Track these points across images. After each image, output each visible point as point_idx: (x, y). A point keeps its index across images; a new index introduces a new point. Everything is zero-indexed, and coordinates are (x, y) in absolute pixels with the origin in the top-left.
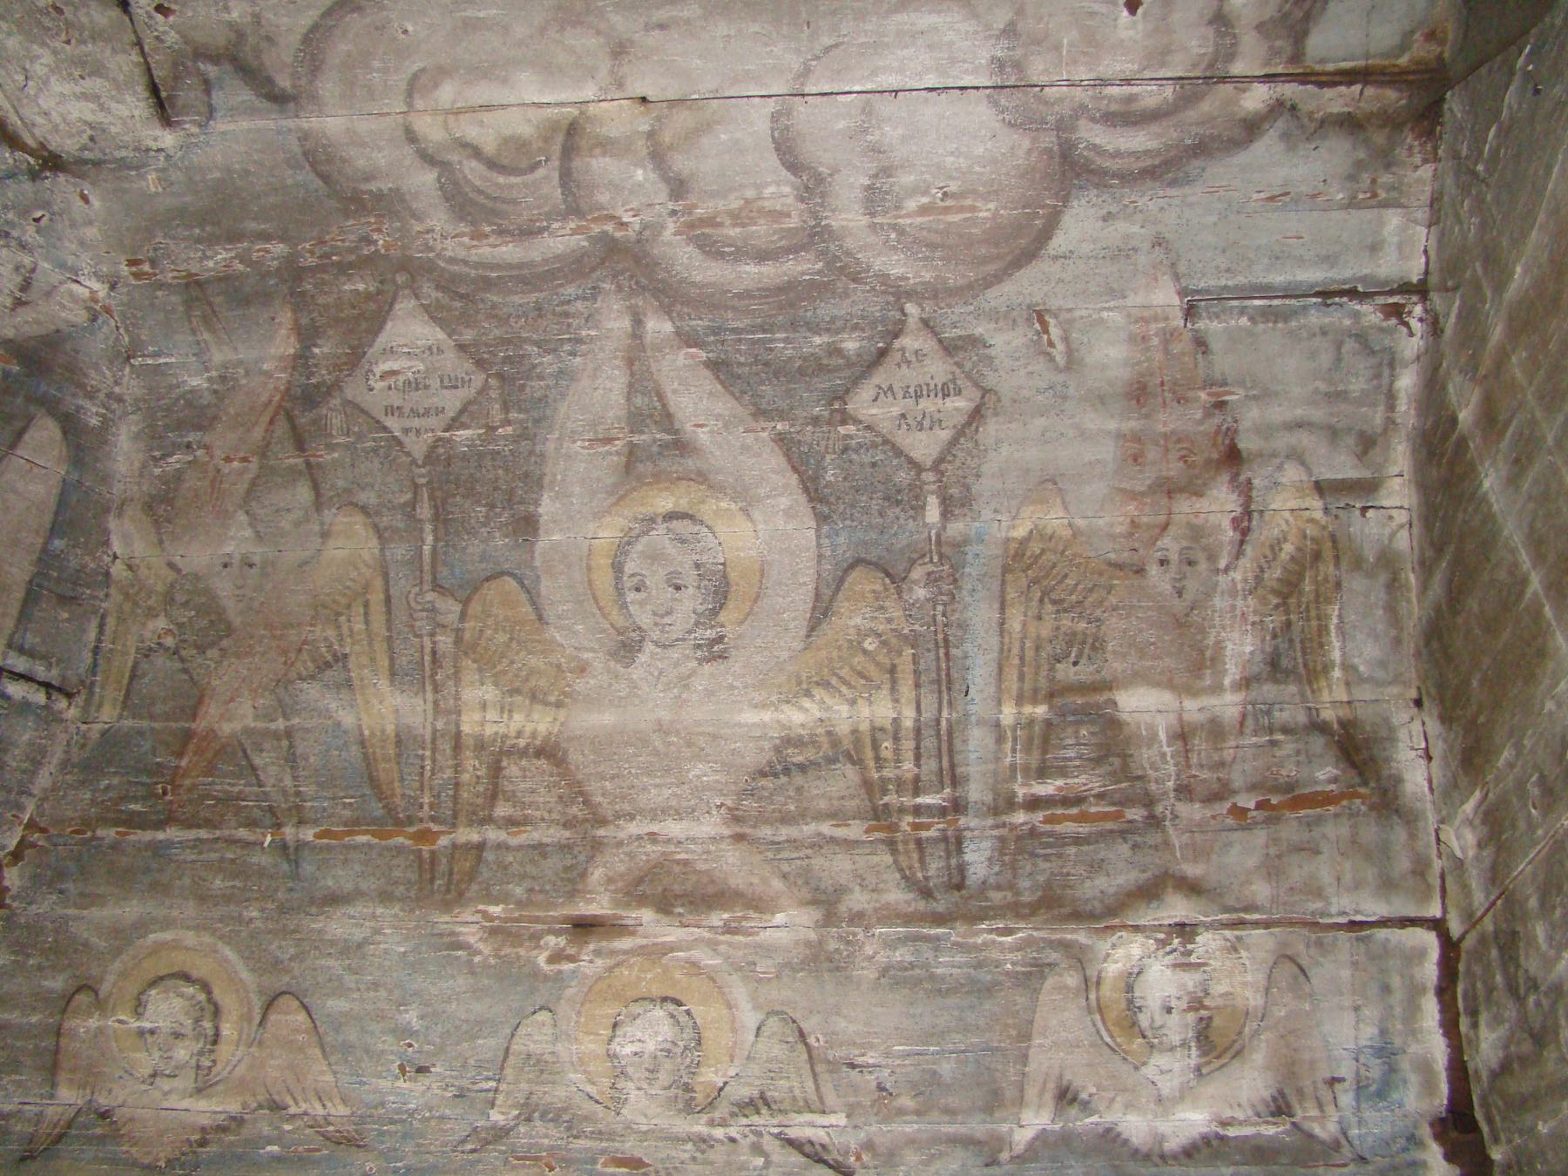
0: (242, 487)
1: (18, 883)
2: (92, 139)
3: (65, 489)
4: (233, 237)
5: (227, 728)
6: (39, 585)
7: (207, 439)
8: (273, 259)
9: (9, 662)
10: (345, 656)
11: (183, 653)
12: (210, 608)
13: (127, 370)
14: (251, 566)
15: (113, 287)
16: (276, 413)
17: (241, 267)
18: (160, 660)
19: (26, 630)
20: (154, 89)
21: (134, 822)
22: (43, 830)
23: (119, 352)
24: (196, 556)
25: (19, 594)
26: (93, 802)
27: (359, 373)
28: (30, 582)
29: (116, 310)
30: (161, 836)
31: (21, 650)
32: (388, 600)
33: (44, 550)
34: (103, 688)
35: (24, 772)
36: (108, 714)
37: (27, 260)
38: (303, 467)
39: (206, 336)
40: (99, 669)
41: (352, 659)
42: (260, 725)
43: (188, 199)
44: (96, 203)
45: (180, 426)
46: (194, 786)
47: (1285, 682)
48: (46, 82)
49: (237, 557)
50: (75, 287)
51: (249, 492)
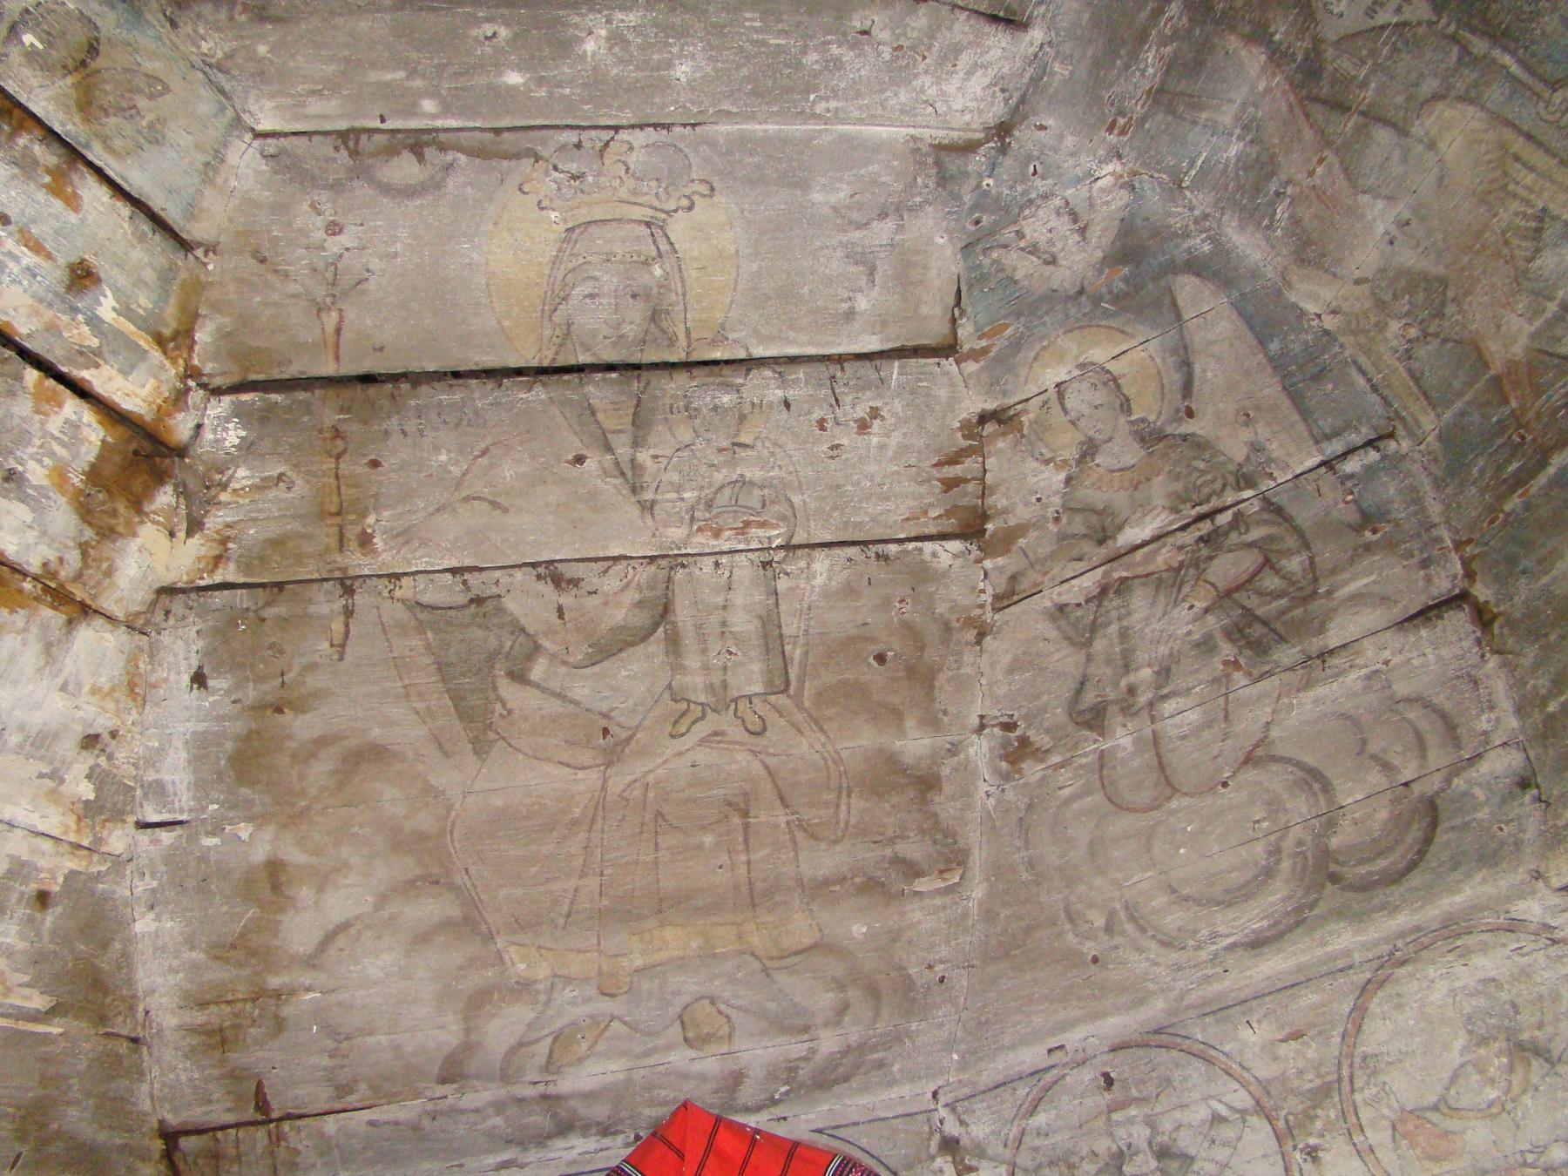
0: (1341, 180)
1: (1489, 592)
2: (1003, 91)
3: (1238, 307)
4: (1142, 37)
5: (1517, 350)
6: (1293, 385)
7: (1283, 177)
8: (1180, 18)
9: (1328, 452)
10: (1544, 210)
11: (1431, 330)
12: (1414, 281)
13: (1188, 193)
14: (1408, 223)
15: (1119, 157)
16: (1303, 107)
17: (1169, 49)
18: (1421, 352)
19: (1315, 421)
20: (994, 19)
21: (1520, 480)
22: (1470, 541)
23: (1171, 190)
24: (1366, 258)
25: (1285, 403)
26: (1482, 491)
27: (1320, 15)
28: (1284, 388)
29: (1137, 167)
30: (1551, 470)
31: (1328, 437)
32: (1529, 137)
33: (1270, 360)
34: (1405, 408)
35: (1416, 513)
36: (1428, 422)
37: (1057, 202)
38: (1362, 120)
39: (1204, 115)
40: (1390, 398)
41: (1551, 206)
42: (1537, 324)
43: (1090, 52)
44: (1050, 122)
45: (1257, 190)
46: (1538, 414)
47: (129, 940)
48: (943, 93)
49: (1392, 228)
50: (1100, 183)
51: (1348, 177)
